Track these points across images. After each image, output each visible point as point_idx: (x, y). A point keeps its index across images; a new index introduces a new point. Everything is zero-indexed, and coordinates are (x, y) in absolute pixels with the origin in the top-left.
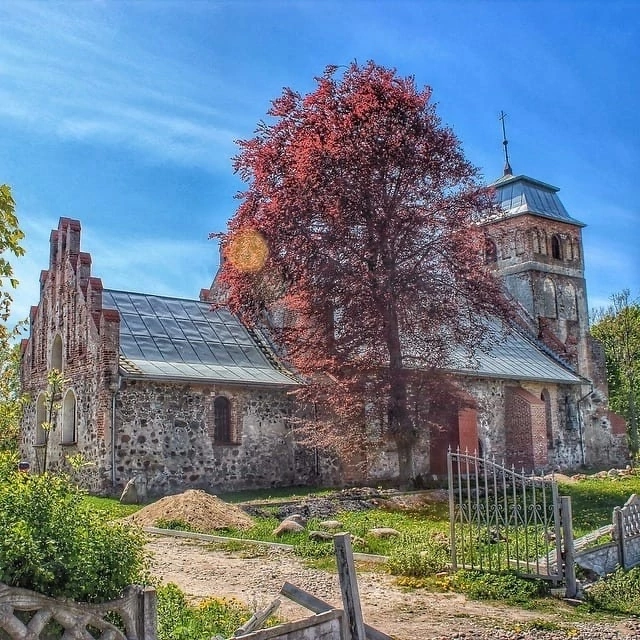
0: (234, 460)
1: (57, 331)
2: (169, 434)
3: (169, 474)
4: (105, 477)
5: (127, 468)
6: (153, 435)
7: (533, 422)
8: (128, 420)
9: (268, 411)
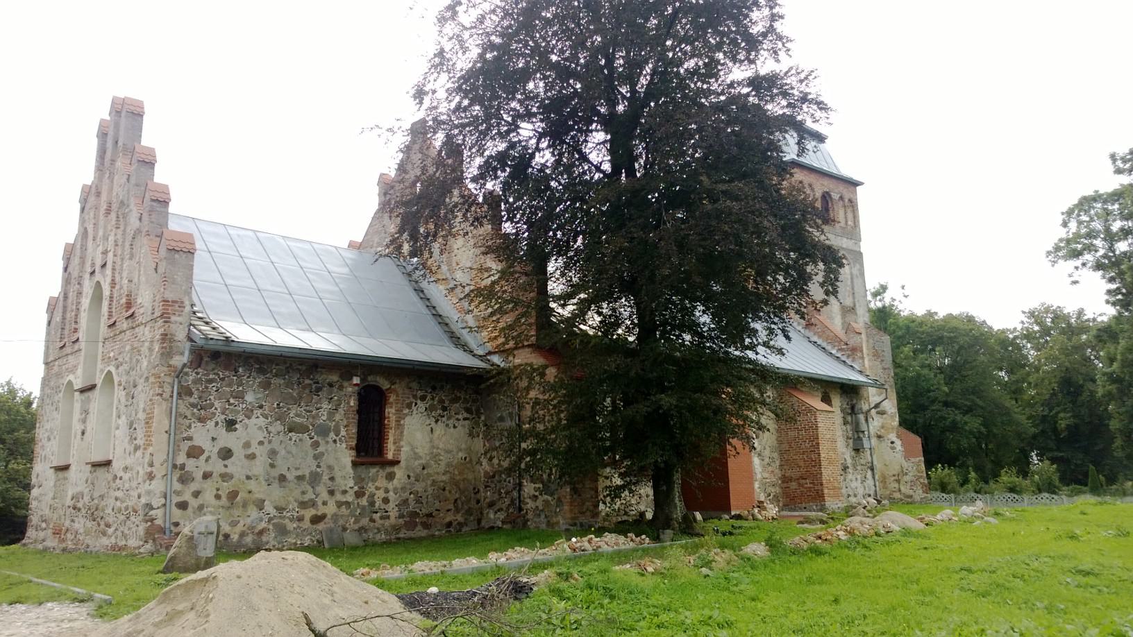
0: (388, 489)
1: (98, 277)
2: (275, 445)
3: (273, 512)
4: (152, 520)
5: (194, 503)
6: (247, 445)
7: (820, 436)
8: (202, 420)
9: (444, 409)
